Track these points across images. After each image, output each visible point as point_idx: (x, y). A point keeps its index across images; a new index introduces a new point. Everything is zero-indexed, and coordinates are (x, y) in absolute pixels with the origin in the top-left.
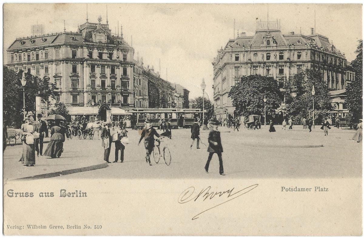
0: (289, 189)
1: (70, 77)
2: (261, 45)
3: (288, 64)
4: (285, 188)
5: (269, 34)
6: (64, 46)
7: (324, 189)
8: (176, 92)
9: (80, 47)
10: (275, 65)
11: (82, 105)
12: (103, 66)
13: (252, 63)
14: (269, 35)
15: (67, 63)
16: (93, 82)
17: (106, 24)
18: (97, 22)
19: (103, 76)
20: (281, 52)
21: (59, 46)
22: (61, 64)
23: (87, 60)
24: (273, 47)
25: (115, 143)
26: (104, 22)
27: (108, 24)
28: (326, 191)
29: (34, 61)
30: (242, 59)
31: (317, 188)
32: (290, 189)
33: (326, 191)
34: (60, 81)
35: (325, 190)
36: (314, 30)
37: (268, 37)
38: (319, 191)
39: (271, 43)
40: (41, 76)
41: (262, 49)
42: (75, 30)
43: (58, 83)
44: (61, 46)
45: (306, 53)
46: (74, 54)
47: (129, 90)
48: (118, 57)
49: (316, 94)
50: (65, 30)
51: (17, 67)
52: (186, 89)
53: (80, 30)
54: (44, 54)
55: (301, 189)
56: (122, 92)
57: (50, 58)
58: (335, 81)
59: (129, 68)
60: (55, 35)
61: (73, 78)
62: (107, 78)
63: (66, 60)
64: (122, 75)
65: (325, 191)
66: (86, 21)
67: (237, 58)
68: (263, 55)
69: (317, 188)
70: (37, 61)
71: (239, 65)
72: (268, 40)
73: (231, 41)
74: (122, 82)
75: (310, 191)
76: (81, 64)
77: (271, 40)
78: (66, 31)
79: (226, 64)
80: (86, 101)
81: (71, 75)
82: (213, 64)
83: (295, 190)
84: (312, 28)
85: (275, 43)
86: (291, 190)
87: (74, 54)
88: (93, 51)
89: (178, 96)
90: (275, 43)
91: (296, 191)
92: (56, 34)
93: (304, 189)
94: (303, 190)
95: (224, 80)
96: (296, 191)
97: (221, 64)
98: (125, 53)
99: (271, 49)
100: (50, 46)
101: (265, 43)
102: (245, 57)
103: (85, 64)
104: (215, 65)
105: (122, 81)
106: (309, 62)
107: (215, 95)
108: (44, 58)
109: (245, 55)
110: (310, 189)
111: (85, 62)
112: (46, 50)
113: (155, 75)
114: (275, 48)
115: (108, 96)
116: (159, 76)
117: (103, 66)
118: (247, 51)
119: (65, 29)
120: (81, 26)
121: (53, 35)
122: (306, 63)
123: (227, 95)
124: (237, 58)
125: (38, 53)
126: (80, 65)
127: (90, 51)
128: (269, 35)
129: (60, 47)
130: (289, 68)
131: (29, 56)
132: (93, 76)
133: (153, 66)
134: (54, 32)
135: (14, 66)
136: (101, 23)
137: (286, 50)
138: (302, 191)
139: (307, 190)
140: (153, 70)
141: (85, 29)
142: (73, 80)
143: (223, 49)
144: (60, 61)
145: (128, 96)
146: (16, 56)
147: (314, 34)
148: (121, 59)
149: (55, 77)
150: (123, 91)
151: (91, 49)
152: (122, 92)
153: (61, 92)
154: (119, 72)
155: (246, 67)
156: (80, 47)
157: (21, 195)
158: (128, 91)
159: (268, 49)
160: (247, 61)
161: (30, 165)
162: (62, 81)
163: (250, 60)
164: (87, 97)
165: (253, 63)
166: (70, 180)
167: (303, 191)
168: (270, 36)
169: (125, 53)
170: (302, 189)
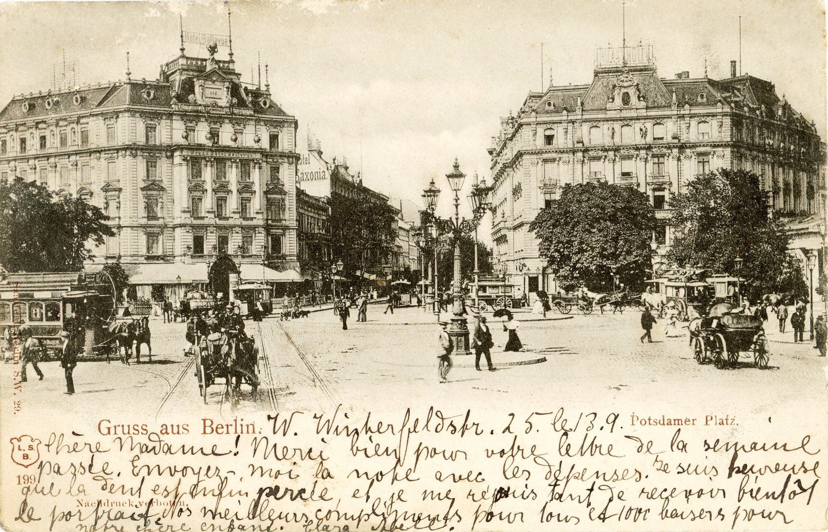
0: (648, 421)
1: (143, 189)
2: (609, 106)
3: (675, 151)
5: (627, 77)
6: (127, 114)
8: (402, 220)
9: (164, 117)
10: (611, 153)
11: (164, 258)
12: (220, 161)
13: (586, 151)
14: (626, 81)
15: (135, 156)
16: (196, 202)
17: (227, 58)
18: (206, 55)
19: (222, 188)
20: (658, 121)
21: (117, 114)
22: (120, 158)
23: (180, 148)
24: (637, 109)
26: (222, 54)
27: (234, 58)
29: (76, 148)
30: (560, 141)
32: (649, 419)
34: (117, 200)
36: (738, 64)
37: (626, 84)
39: (634, 100)
40: (72, 187)
41: (611, 114)
42: (152, 75)
43: (113, 205)
44: (120, 115)
45: (688, 125)
47: (285, 220)
48: (256, 139)
49: (778, 237)
50: (130, 76)
51: (55, 163)
53: (164, 73)
54: (80, 133)
55: (675, 420)
56: (268, 225)
57: (93, 143)
58: (792, 192)
59: (286, 165)
60: (105, 88)
61: (149, 192)
62: (230, 191)
63: (132, 149)
64: (267, 184)
66: (180, 53)
67: (549, 139)
68: (613, 128)
70: (22, 155)
71: (554, 155)
72: (624, 93)
73: (533, 97)
74: (268, 200)
75: (693, 424)
76: (167, 157)
77: (632, 91)
78: (132, 77)
79: (520, 155)
80: (179, 249)
81: (143, 185)
82: (491, 153)
83: (662, 422)
84: (732, 62)
85: (642, 99)
88: (245, 128)
89: (407, 227)
90: (642, 99)
92: (108, 86)
93: (680, 421)
95: (517, 191)
96: (664, 424)
97: (508, 155)
98: (152, 123)
99: (633, 114)
100: (93, 115)
101: (618, 101)
102: (569, 136)
103: (177, 159)
104: (494, 155)
105: (267, 198)
106: (726, 146)
107: (496, 229)
108: (80, 143)
109: (570, 131)
111: (177, 154)
112: (83, 124)
113: (350, 179)
114: (643, 113)
116: (361, 181)
117: (220, 161)
118: (573, 122)
119: (130, 74)
120: (167, 65)
121: (102, 86)
122: (720, 149)
123: (526, 228)
124: (549, 139)
125: (85, 129)
126: (164, 159)
127: (238, 128)
128: (626, 81)
129: (117, 117)
130: (679, 159)
131: (23, 141)
132: (196, 188)
133: (345, 158)
134: (104, 83)
135: (28, 162)
136: (217, 57)
137: (669, 117)
138: (675, 424)
139: (687, 423)
140: (346, 168)
141: (176, 71)
142: (148, 197)
143: (515, 115)
144: (118, 150)
145: (284, 235)
146: (13, 139)
147: (738, 75)
148: (265, 144)
149: (106, 189)
150: (270, 222)
151: (239, 125)
152: (268, 225)
153: (119, 227)
154: (258, 178)
155: (571, 160)
156: (164, 117)
158: (284, 222)
159: (625, 114)
160: (574, 145)
161: (130, 350)
162: (121, 199)
163: (582, 142)
164: (182, 240)
165: (589, 150)
168: (630, 83)
169: (152, 123)
170: (677, 422)
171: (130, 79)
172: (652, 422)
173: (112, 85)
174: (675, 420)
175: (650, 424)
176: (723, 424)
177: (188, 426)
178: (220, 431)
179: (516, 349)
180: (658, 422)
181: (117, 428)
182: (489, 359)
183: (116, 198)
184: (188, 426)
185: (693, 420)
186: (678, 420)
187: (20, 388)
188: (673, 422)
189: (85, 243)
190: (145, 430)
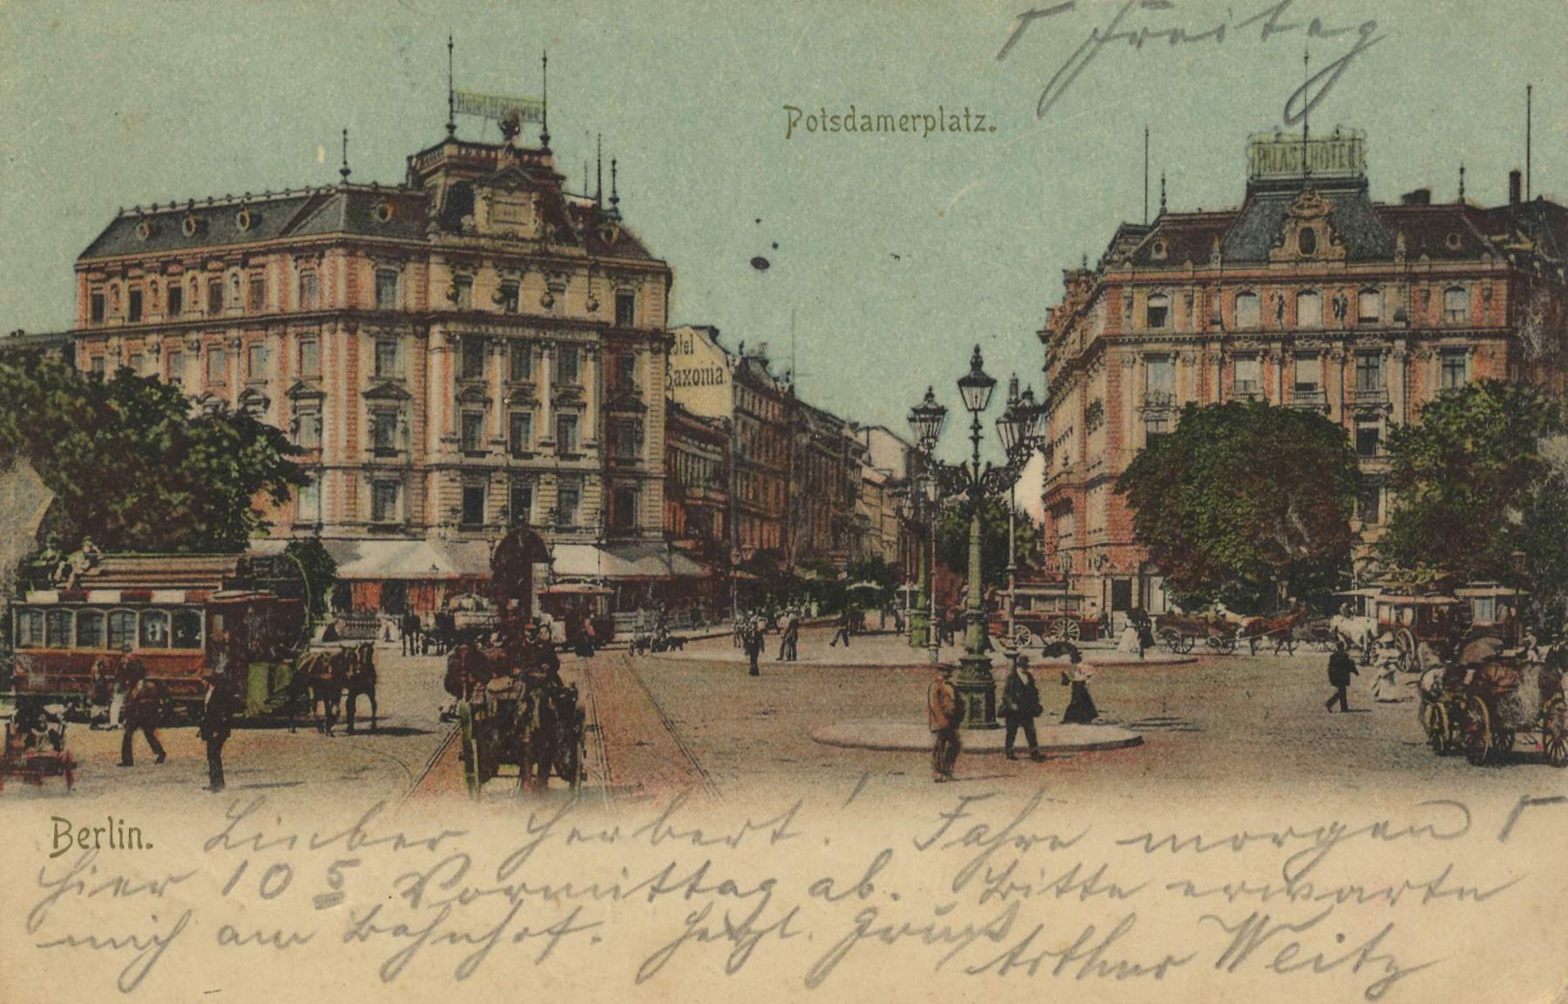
78: (351, 179)
171: (347, 183)
173: (312, 193)
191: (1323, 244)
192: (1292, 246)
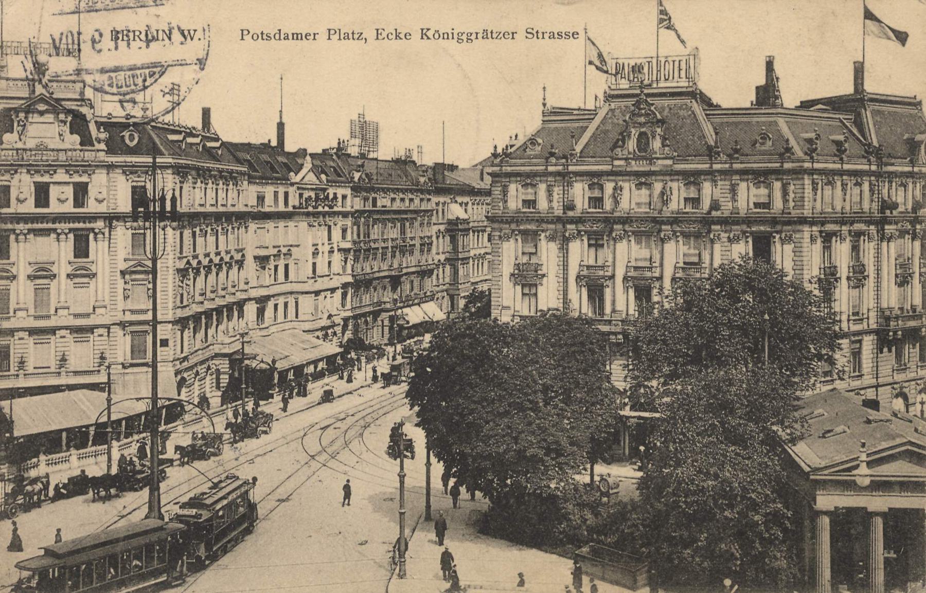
0: (260, 36)
4: (249, 32)
7: (353, 33)
25: (589, 482)
28: (358, 39)
31: (333, 32)
32: (262, 33)
33: (358, 39)
35: (356, 36)
38: (340, 39)
46: (763, 247)
52: (248, 531)
65: (353, 39)
69: (333, 32)
86: (265, 37)
87: (763, 247)
91: (280, 39)
94: (297, 36)
110: (513, 33)
115: (16, 342)
139: (575, 36)
157: (552, 36)
166: (490, 548)
167: (297, 39)
172: (265, 37)
174: (293, 34)
175: (263, 39)
176: (288, 39)
177: (527, 37)
178: (390, 37)
179: (20, 549)
180: (272, 36)
181: (545, 34)
182: (349, 501)
183: (222, 370)
184: (527, 37)
185: (314, 34)
186: (297, 34)
187: (192, 32)
188: (290, 37)
189: (426, 335)
190: (530, 33)
191: (656, 144)
192: (632, 144)
